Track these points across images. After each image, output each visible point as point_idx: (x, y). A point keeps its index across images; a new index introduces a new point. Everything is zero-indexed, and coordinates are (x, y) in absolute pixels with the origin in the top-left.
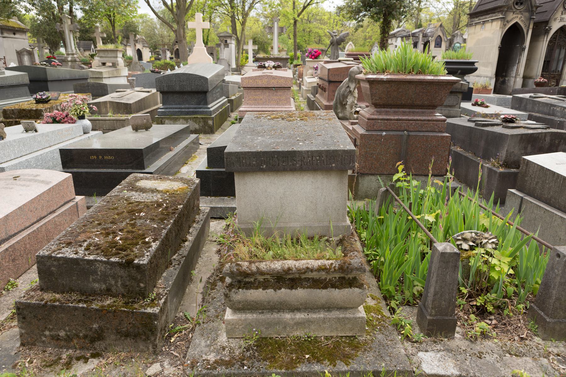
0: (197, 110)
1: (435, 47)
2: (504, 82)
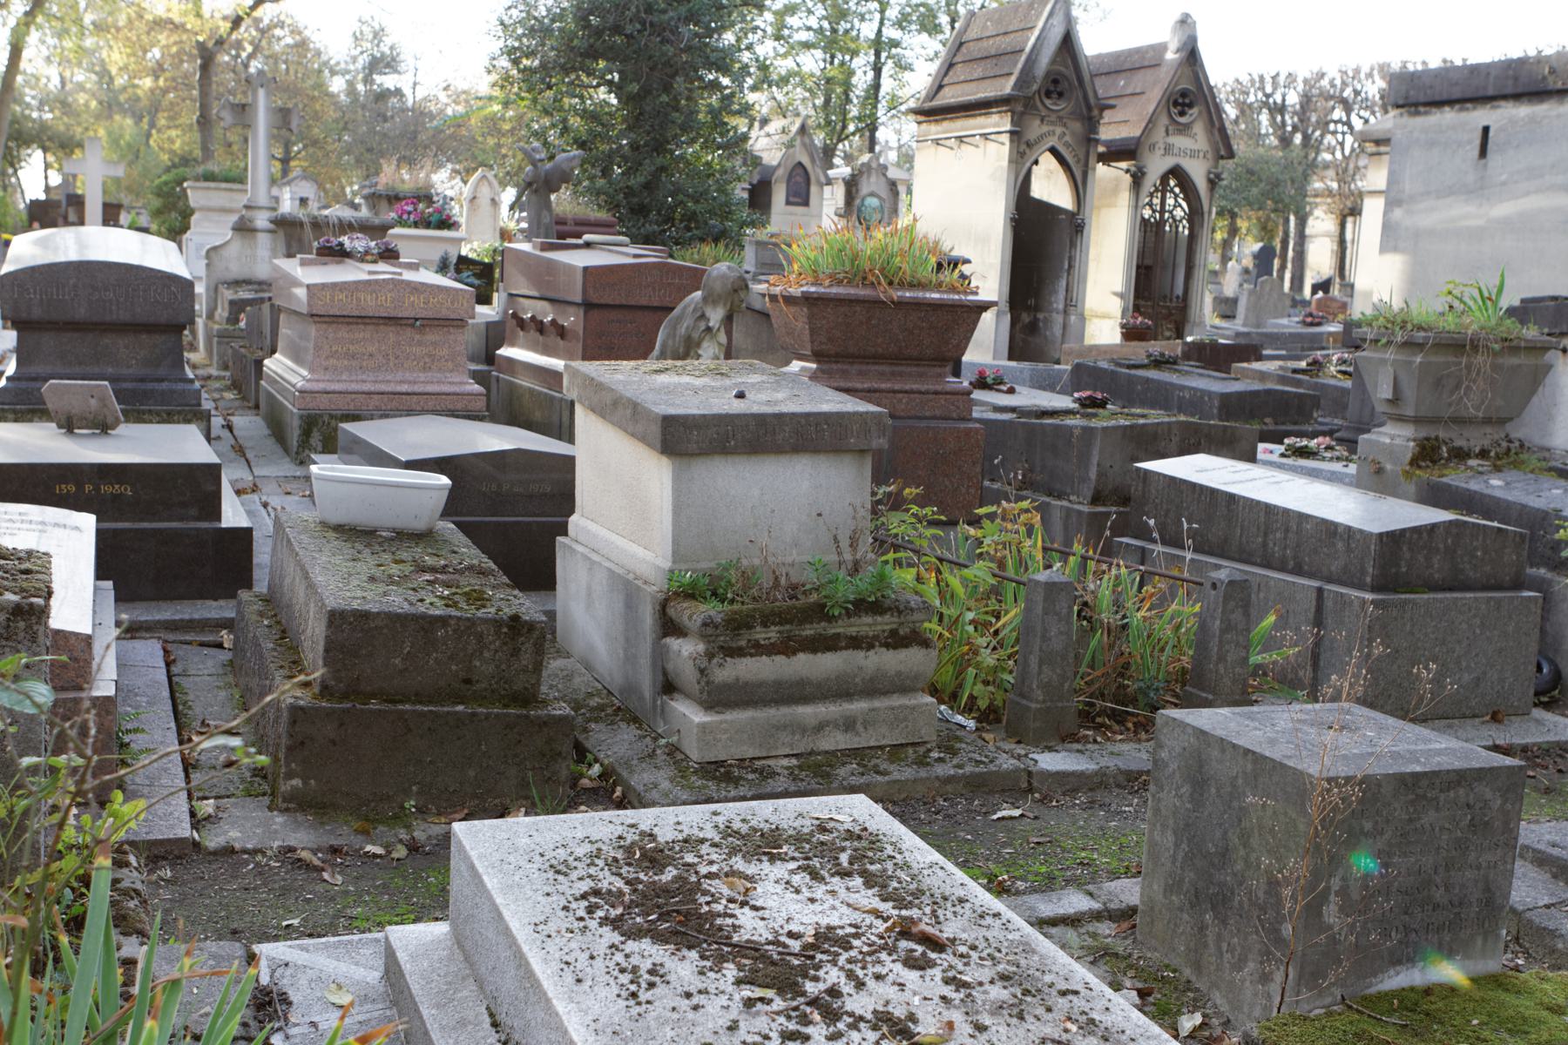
0: (150, 386)
1: (788, 203)
2: (1033, 328)
